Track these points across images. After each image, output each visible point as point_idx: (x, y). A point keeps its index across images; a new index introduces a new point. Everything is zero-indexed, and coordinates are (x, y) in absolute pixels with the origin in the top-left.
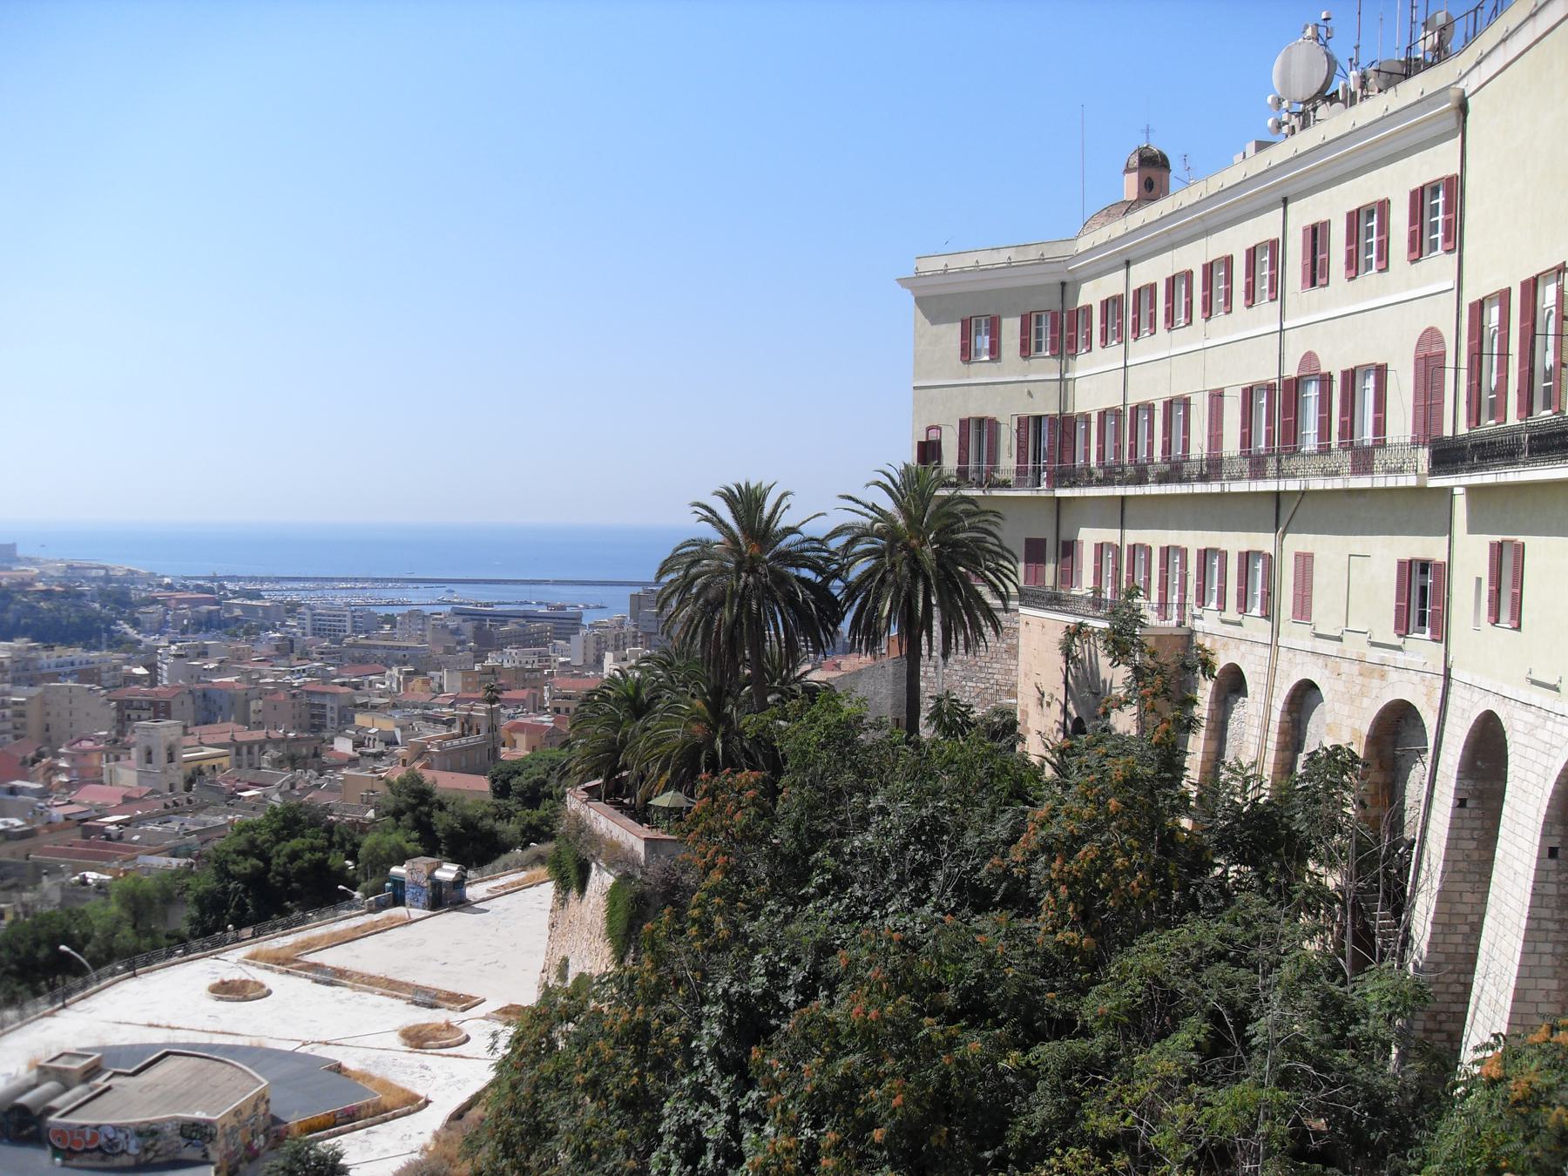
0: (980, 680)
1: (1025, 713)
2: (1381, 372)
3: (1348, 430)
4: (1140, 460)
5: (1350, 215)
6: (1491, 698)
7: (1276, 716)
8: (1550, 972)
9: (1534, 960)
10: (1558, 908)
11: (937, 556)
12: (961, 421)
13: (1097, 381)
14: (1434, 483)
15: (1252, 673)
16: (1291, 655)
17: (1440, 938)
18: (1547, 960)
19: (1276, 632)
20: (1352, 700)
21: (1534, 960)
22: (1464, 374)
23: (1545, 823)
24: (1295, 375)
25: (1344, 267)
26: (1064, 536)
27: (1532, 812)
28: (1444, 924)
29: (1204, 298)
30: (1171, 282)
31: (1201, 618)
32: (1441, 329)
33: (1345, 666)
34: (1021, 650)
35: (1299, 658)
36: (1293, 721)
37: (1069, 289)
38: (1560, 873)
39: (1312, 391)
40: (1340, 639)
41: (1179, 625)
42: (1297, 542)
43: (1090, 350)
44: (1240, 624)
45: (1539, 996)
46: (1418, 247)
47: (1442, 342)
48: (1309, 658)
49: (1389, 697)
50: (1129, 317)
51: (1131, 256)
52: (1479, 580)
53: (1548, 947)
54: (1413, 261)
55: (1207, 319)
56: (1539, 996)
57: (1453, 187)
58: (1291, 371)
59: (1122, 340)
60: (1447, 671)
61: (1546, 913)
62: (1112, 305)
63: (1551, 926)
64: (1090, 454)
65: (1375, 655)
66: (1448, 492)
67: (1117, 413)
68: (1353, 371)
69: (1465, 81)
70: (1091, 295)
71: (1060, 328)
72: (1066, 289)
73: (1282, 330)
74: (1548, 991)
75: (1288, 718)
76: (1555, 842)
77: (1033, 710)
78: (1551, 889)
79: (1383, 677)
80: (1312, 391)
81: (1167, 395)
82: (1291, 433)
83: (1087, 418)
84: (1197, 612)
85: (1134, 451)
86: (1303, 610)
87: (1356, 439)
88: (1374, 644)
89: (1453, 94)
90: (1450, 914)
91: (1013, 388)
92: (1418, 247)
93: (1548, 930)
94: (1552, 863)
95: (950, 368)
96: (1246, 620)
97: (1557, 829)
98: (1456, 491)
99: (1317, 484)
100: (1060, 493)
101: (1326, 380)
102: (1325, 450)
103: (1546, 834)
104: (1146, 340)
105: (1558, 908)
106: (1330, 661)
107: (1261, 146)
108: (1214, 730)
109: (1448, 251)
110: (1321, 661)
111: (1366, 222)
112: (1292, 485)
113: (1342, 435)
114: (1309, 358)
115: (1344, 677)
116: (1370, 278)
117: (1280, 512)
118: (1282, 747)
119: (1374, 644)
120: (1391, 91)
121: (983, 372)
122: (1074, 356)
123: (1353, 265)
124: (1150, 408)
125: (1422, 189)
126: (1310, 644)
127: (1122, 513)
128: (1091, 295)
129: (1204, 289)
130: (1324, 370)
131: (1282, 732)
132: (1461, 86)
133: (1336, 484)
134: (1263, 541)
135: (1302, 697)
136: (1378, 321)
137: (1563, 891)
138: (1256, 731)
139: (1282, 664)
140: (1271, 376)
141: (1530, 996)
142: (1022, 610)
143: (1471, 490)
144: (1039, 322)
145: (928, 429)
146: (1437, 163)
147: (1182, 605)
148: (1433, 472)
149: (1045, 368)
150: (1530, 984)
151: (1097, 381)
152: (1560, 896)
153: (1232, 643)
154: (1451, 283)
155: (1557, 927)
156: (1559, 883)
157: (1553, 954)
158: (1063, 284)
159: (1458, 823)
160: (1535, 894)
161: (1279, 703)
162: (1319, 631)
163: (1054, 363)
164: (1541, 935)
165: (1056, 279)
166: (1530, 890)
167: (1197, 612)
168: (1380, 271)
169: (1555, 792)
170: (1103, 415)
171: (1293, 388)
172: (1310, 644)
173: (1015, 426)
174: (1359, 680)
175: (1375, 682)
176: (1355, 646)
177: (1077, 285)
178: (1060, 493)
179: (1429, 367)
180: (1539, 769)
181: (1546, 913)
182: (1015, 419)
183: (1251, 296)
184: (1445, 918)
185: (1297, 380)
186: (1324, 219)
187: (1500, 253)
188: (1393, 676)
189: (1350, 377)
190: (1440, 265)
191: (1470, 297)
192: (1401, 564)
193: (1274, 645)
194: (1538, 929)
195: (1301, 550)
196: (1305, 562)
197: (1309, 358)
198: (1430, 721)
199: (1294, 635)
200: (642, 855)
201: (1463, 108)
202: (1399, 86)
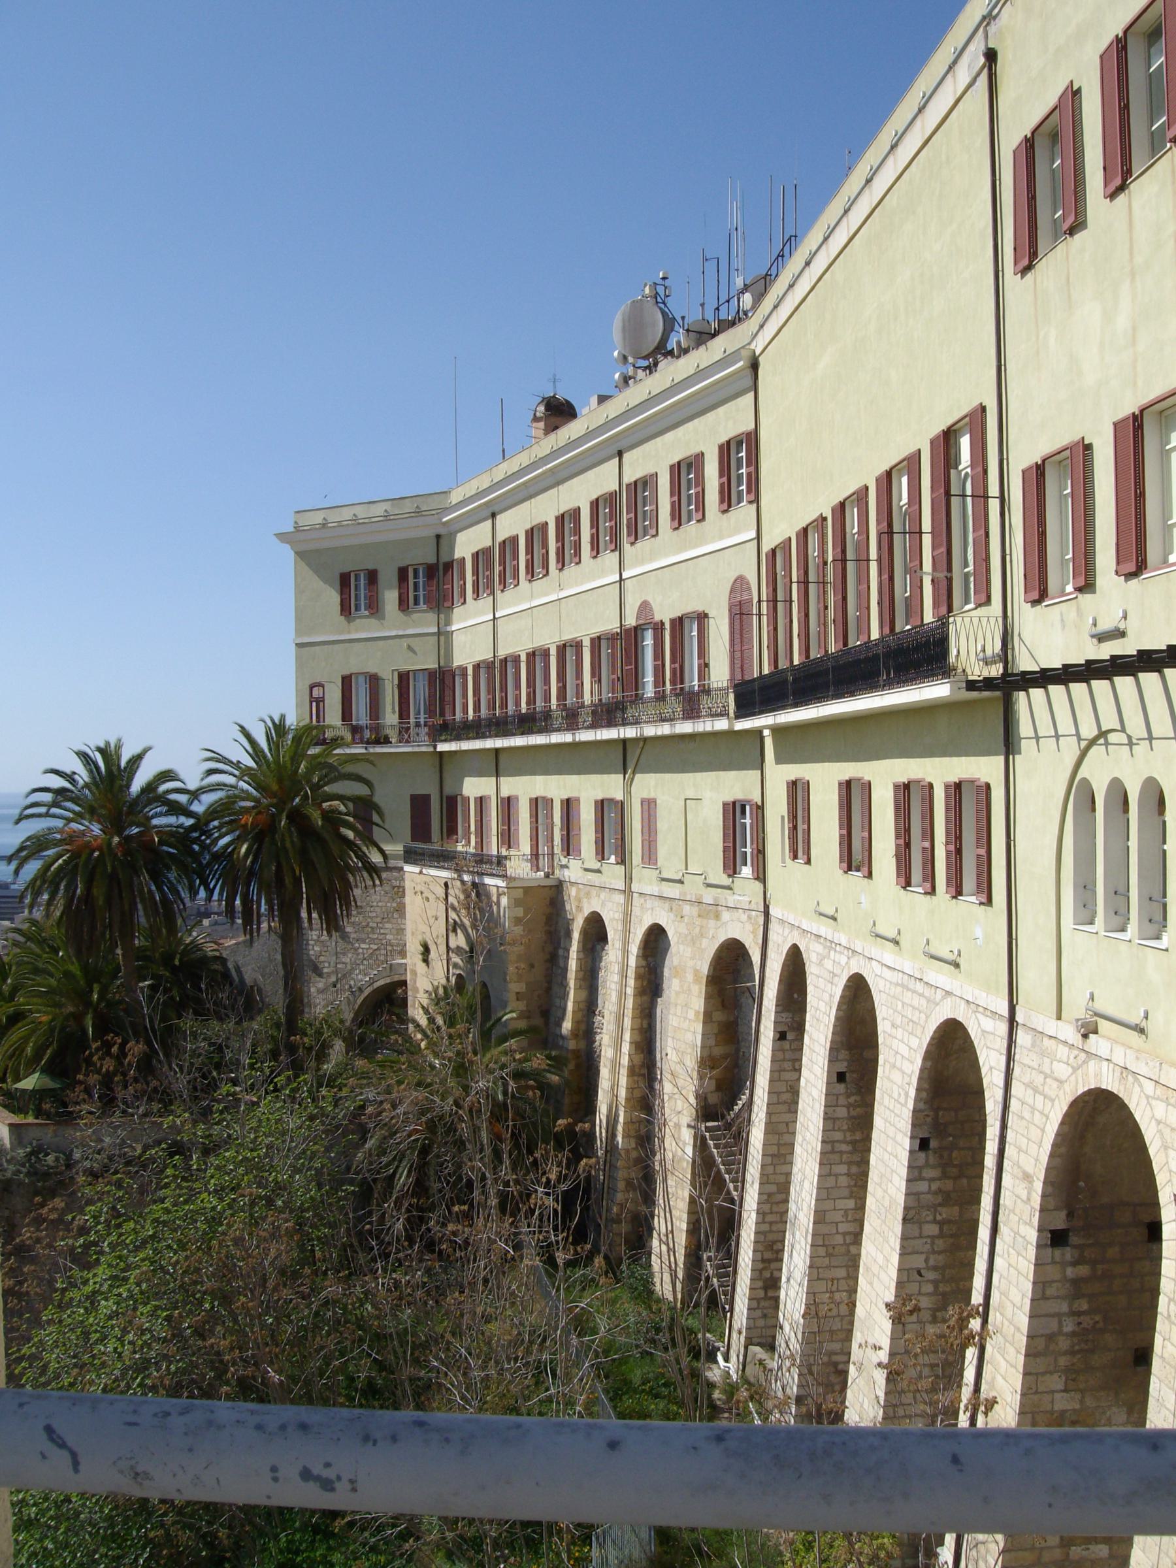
0: (372, 941)
1: (414, 973)
2: (702, 617)
3: (679, 675)
4: (517, 707)
5: (672, 467)
6: (796, 933)
7: (632, 962)
8: (846, 1192)
9: (831, 1182)
10: (849, 1130)
11: (300, 829)
12: (343, 678)
13: (478, 631)
14: (741, 725)
15: (612, 920)
16: (642, 900)
17: (770, 1169)
18: (843, 1181)
19: (629, 879)
20: (693, 941)
21: (831, 1182)
22: (764, 619)
23: (831, 1049)
24: (634, 624)
25: (669, 518)
26: (448, 791)
27: (822, 1040)
28: (772, 1156)
29: (527, 561)
30: (530, 533)
31: (566, 867)
32: (749, 577)
33: (687, 909)
34: (408, 908)
35: (649, 903)
36: (648, 965)
37: (443, 542)
38: (848, 1097)
39: (649, 641)
40: (681, 882)
41: (547, 876)
42: (647, 784)
43: (464, 602)
44: (599, 871)
45: (838, 1216)
46: (727, 500)
47: (749, 589)
48: (657, 903)
49: (722, 938)
50: (498, 568)
51: (496, 509)
52: (783, 817)
53: (843, 1169)
54: (725, 512)
55: (561, 570)
56: (838, 1216)
57: (751, 440)
58: (631, 621)
59: (617, 547)
60: (766, 907)
61: (838, 1136)
62: (482, 557)
63: (844, 1147)
64: (467, 707)
65: (709, 896)
66: (758, 733)
67: (490, 666)
68: (681, 619)
69: (754, 343)
70: (466, 545)
71: (432, 580)
72: (442, 540)
73: (621, 579)
74: (846, 1211)
75: (644, 963)
76: (842, 1067)
77: (421, 967)
78: (842, 1112)
79: (717, 917)
80: (649, 641)
81: (529, 646)
82: (632, 679)
83: (464, 670)
84: (564, 861)
85: (562, 691)
86: (650, 856)
87: (687, 685)
88: (709, 885)
89: (744, 353)
90: (779, 1145)
91: (392, 641)
92: (727, 500)
93: (841, 1152)
94: (841, 1088)
95: (333, 627)
96: (605, 868)
97: (844, 1054)
98: (766, 732)
99: (650, 731)
100: (442, 747)
101: (659, 628)
102: (660, 697)
103: (833, 1059)
104: (510, 593)
105: (849, 1130)
106: (675, 904)
107: (602, 399)
108: (584, 979)
109: (750, 502)
110: (667, 905)
111: (686, 471)
112: (630, 732)
113: (673, 683)
114: (645, 607)
115: (686, 919)
116: (691, 528)
117: (626, 758)
118: (640, 992)
119: (709, 885)
120: (702, 348)
121: (364, 628)
122: (451, 608)
123: (678, 518)
124: (546, 653)
125: (728, 442)
126: (654, 888)
127: (497, 764)
128: (466, 545)
129: (527, 554)
130: (657, 618)
131: (638, 977)
132: (752, 346)
133: (665, 729)
134: (610, 785)
135: (656, 941)
136: (694, 571)
137: (853, 1113)
138: (616, 978)
139: (636, 911)
140: (613, 626)
141: (830, 1217)
142: (407, 868)
143: (777, 730)
144: (416, 576)
145: (311, 688)
146: (731, 420)
147: (552, 855)
148: (739, 716)
149: (423, 623)
150: (828, 1205)
151: (478, 631)
152: (851, 1118)
153: (594, 892)
154: (753, 534)
155: (849, 1148)
156: (848, 1106)
157: (848, 1175)
158: (438, 537)
159: (780, 1055)
160: (826, 1118)
161: (634, 949)
162: (665, 875)
163: (431, 616)
164: (836, 1157)
165: (431, 532)
166: (822, 1115)
167: (564, 861)
168: (698, 521)
169: (837, 1018)
170: (477, 667)
171: (635, 634)
172: (654, 888)
173: (396, 682)
174: (698, 922)
175: (712, 923)
176: (694, 887)
177: (452, 537)
178: (442, 747)
179: (739, 613)
180: (826, 997)
181: (838, 1136)
182: (396, 674)
183: (476, 591)
184: (774, 1150)
185: (636, 628)
186: (653, 471)
187: (795, 498)
188: (726, 915)
189: (678, 623)
190: (744, 512)
191: (766, 547)
192: (725, 805)
193: (628, 892)
194: (833, 1152)
195: (645, 796)
196: (649, 805)
197: (645, 607)
198: (756, 958)
199: (645, 881)
200: (8, 1146)
201: (754, 366)
202: (709, 344)
